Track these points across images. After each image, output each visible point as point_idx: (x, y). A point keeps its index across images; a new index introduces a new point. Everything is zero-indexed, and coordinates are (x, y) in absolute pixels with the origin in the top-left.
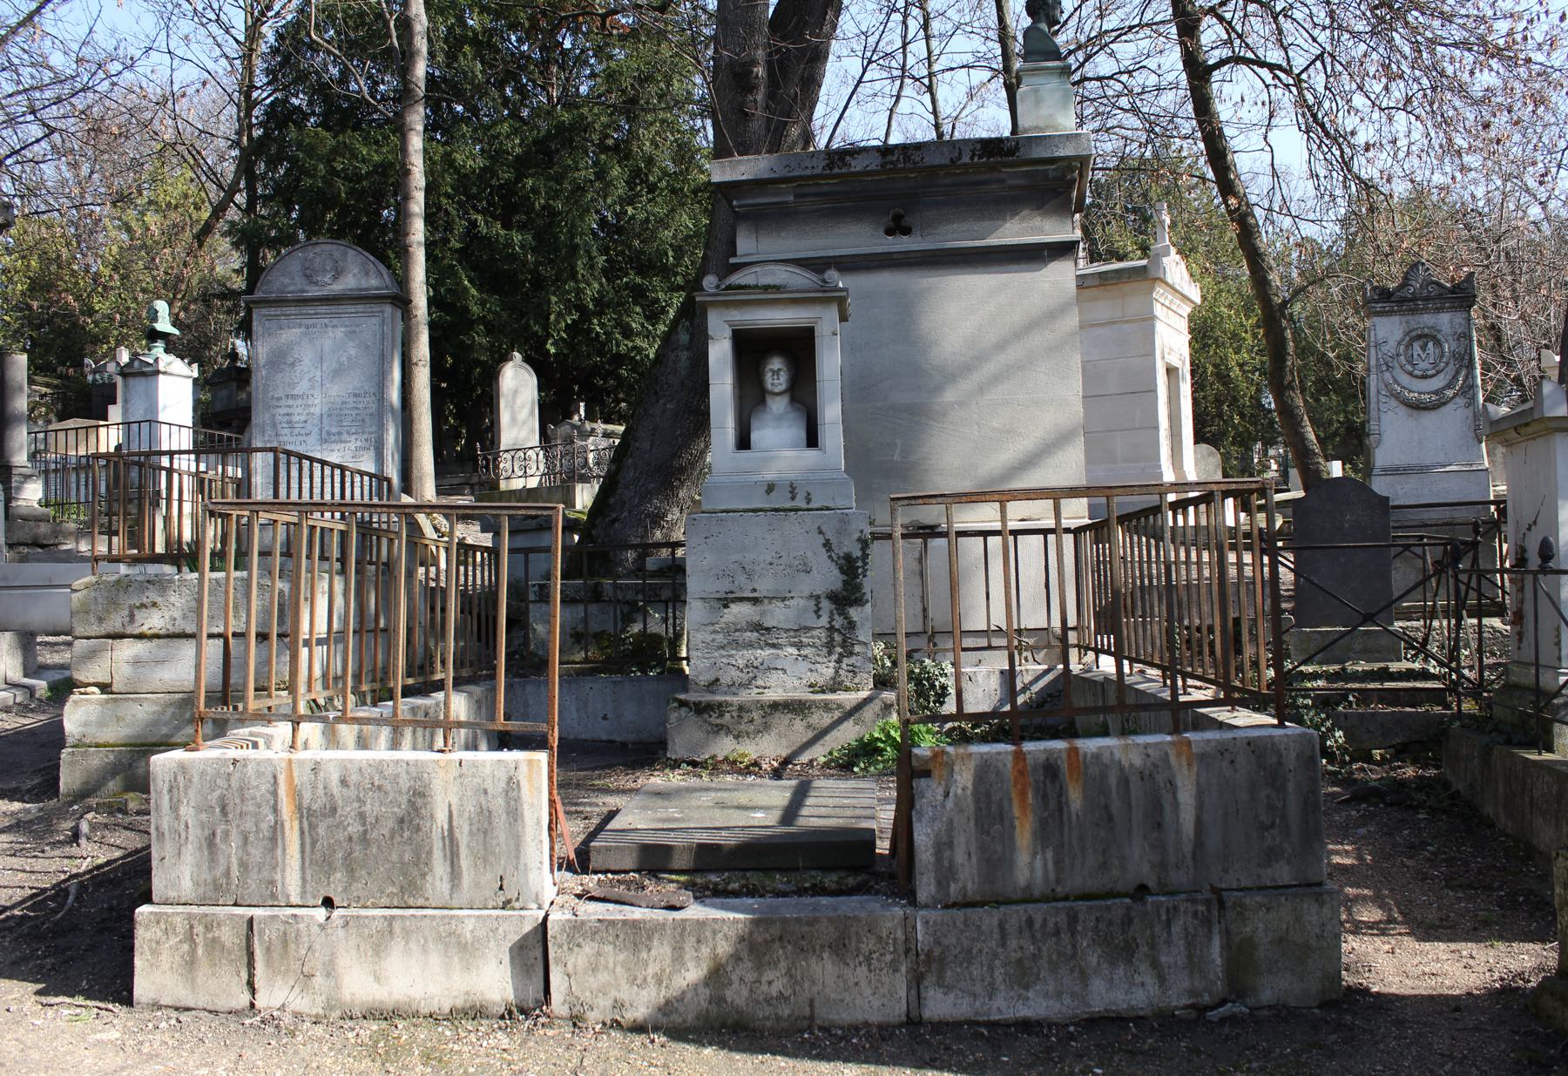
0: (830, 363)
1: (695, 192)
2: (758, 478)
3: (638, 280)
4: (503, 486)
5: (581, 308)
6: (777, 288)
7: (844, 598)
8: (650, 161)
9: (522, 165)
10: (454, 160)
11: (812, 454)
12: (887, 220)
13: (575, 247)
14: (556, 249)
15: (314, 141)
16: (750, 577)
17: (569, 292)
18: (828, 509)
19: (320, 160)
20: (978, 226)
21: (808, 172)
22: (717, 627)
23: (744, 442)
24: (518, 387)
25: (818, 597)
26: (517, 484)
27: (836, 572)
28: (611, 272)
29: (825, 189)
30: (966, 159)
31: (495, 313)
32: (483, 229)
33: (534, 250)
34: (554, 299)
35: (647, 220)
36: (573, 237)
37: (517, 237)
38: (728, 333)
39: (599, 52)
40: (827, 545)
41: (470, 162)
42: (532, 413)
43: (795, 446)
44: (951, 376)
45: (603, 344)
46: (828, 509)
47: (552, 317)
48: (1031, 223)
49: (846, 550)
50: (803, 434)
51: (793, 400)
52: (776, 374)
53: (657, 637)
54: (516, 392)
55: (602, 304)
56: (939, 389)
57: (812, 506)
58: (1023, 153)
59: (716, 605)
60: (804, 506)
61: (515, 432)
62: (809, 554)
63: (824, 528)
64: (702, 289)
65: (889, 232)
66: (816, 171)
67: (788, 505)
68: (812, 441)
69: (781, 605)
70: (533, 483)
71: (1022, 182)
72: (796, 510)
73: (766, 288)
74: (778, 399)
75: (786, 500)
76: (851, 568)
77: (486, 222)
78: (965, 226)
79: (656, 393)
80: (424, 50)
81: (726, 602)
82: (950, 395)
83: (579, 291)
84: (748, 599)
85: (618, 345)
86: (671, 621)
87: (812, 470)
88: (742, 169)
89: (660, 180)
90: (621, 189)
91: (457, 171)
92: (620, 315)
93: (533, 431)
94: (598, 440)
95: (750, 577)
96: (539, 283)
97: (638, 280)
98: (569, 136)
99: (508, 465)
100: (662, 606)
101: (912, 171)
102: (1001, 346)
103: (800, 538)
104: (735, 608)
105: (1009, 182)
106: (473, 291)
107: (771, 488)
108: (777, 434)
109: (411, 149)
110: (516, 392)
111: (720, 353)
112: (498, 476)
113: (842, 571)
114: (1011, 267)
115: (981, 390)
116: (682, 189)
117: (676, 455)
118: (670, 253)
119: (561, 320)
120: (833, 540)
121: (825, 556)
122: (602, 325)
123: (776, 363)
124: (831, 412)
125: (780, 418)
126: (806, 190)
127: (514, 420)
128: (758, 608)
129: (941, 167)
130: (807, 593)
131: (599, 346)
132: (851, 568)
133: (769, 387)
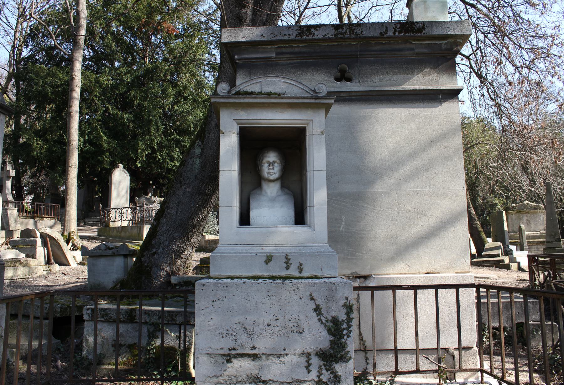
0: (317, 158)
1: (204, 101)
3: (178, 137)
4: (111, 224)
5: (153, 148)
6: (278, 95)
7: (331, 355)
8: (185, 88)
9: (131, 86)
10: (99, 81)
11: (300, 230)
13: (151, 121)
14: (143, 123)
15: (38, 70)
16: (250, 335)
17: (147, 140)
18: (317, 277)
19: (41, 78)
20: (396, 78)
21: (286, 38)
24: (121, 180)
25: (308, 355)
26: (118, 224)
27: (325, 333)
28: (166, 133)
29: (296, 50)
30: (390, 33)
31: (115, 148)
32: (111, 111)
33: (133, 122)
34: (141, 143)
35: (183, 111)
36: (149, 116)
37: (126, 116)
38: (236, 129)
39: (165, 43)
40: (317, 309)
41: (107, 82)
42: (127, 192)
43: (286, 224)
44: (377, 174)
45: (161, 164)
46: (317, 277)
47: (139, 151)
48: (430, 77)
49: (333, 314)
51: (283, 186)
52: (271, 165)
53: (172, 349)
54: (120, 182)
55: (161, 146)
56: (371, 183)
57: (304, 274)
58: (427, 31)
59: (220, 360)
60: (297, 274)
61: (118, 200)
62: (302, 317)
63: (315, 296)
65: (337, 79)
66: (292, 37)
67: (283, 273)
68: (300, 218)
69: (276, 360)
70: (125, 224)
71: (425, 51)
72: (291, 278)
73: (269, 94)
74: (272, 184)
75: (282, 271)
76: (337, 330)
77: (112, 109)
78: (388, 77)
79: (181, 182)
81: (228, 358)
82: (379, 187)
83: (152, 141)
84: (248, 355)
85: (168, 164)
86: (182, 338)
87: (304, 245)
88: (243, 34)
89: (189, 96)
90: (172, 98)
91: (101, 86)
92: (169, 151)
93: (127, 200)
94: (155, 204)
95: (250, 335)
96: (135, 136)
97: (178, 137)
98: (151, 74)
99: (114, 215)
100: (177, 328)
101: (354, 39)
102: (413, 155)
103: (294, 302)
104: (236, 363)
105: (416, 51)
106: (105, 138)
107: (269, 259)
108: (271, 210)
109: (75, 69)
110: (120, 182)
111: (229, 145)
112: (109, 220)
113: (330, 332)
114: (418, 104)
115: (400, 184)
116: (198, 100)
117: (191, 218)
118: (192, 126)
119: (143, 151)
120: (323, 305)
121: (315, 319)
122: (161, 155)
123: (272, 157)
124: (318, 197)
126: (284, 50)
127: (118, 195)
128: (257, 363)
129: (374, 38)
130: (299, 351)
131: (160, 165)
132: (337, 330)
133: (266, 175)
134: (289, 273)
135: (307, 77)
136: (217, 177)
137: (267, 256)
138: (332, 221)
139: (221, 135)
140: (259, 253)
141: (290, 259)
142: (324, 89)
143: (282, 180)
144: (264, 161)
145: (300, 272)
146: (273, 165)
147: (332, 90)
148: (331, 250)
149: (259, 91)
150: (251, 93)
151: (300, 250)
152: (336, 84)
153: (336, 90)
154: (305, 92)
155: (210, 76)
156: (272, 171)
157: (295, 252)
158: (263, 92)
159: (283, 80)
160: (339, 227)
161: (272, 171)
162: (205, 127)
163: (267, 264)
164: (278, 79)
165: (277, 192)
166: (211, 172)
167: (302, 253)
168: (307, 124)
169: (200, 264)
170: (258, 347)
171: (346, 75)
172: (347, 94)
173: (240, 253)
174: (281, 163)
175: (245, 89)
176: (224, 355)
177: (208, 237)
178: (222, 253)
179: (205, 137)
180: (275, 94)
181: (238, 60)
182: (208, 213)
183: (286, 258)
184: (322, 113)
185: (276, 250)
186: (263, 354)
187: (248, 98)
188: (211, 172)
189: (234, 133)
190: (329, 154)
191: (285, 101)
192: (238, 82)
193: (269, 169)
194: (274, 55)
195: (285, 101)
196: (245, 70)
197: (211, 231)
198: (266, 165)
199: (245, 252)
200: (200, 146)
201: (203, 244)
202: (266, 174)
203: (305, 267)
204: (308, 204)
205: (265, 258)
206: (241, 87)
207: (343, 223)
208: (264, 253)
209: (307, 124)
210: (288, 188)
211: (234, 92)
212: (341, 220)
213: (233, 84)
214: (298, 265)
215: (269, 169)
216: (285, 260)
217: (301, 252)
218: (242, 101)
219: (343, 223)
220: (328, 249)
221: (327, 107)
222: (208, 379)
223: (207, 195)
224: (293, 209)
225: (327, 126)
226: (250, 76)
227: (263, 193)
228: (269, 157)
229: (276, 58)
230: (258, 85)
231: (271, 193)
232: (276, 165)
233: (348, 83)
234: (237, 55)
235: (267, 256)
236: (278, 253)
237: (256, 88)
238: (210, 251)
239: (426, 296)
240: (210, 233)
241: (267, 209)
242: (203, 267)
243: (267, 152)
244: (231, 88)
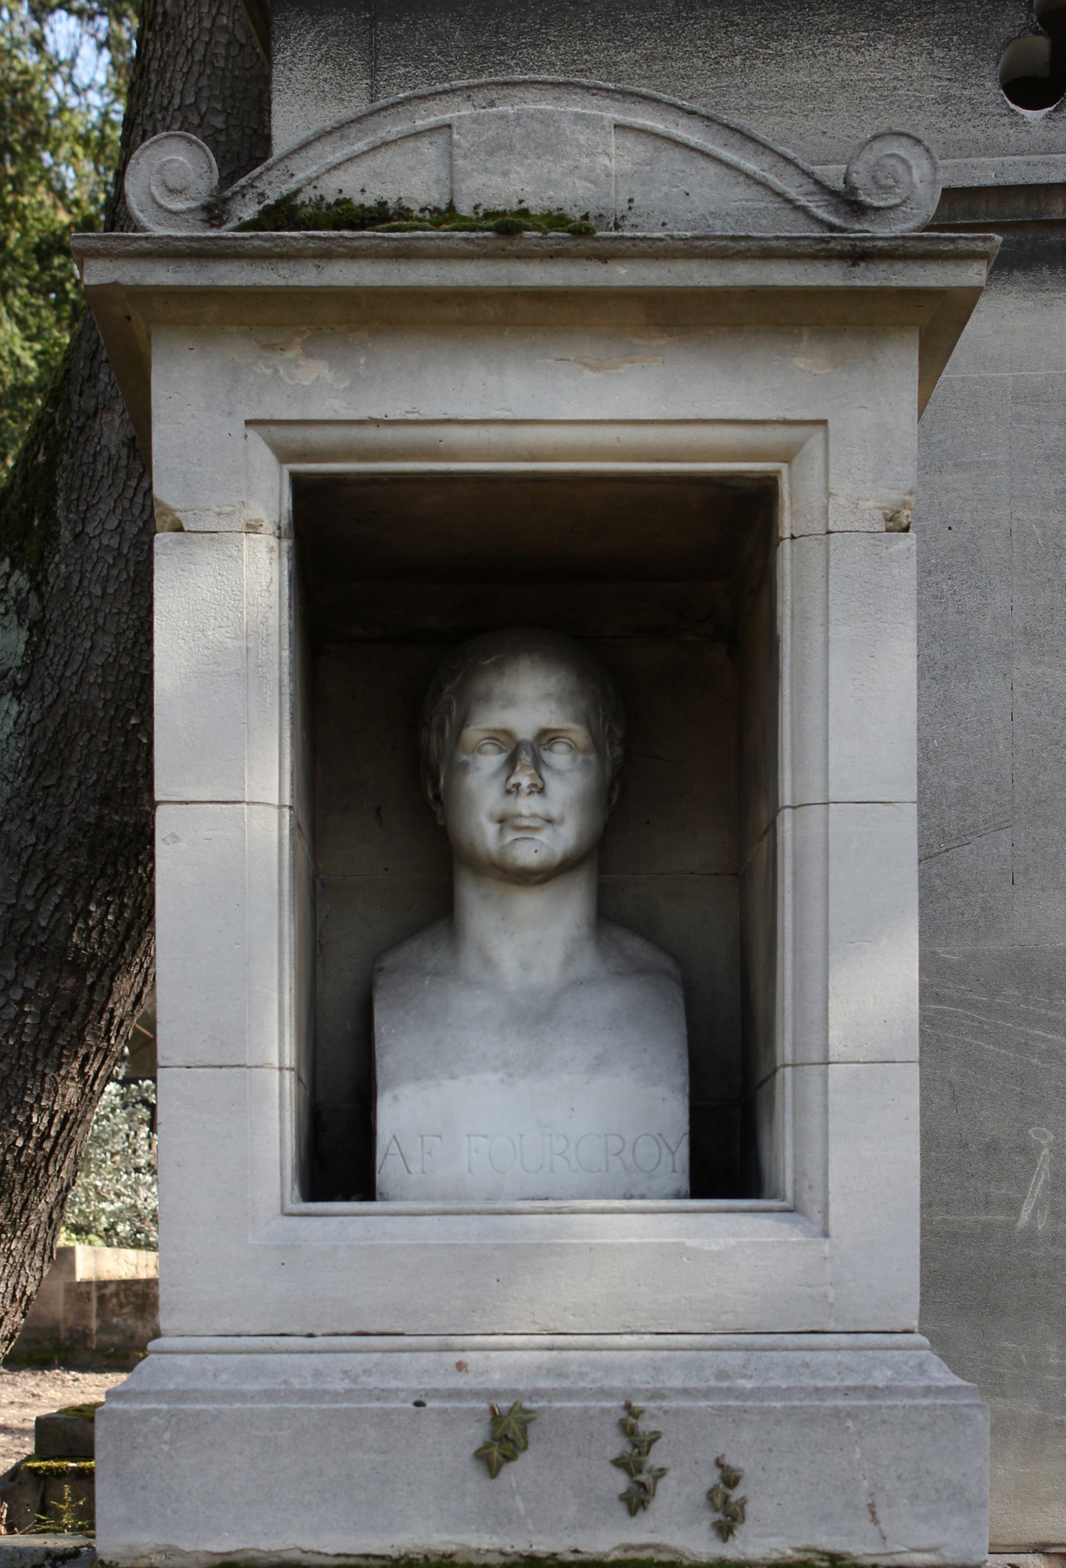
0: (855, 707)
2: (420, 1370)
6: (576, 233)
11: (726, 1231)
23: (338, 1157)
38: (270, 499)
50: (672, 1112)
51: (608, 917)
52: (525, 761)
65: (1026, 90)
68: (728, 1152)
73: (507, 228)
74: (529, 903)
87: (754, 1336)
107: (505, 1438)
108: (525, 1087)
111: (220, 611)
123: (528, 700)
124: (858, 989)
125: (538, 1015)
133: (484, 832)
134: (645, 1538)
135: (801, 76)
136: (141, 841)
137: (496, 1417)
138: (956, 1162)
139: (162, 541)
140: (436, 1393)
141: (655, 1436)
142: (914, 186)
143: (603, 869)
144: (473, 734)
145: (725, 1530)
146: (538, 763)
147: (986, 171)
148: (942, 1375)
149: (437, 198)
150: (379, 216)
151: (722, 1375)
152: (1018, 123)
153: (1012, 178)
154: (773, 204)
155: (88, 50)
156: (527, 805)
157: (686, 1392)
158: (464, 208)
159: (613, 113)
160: (1013, 1207)
161: (527, 805)
162: (52, 463)
163: (493, 1471)
164: (576, 105)
165: (569, 960)
166: (105, 800)
167: (742, 1394)
168: (787, 455)
169: (41, 1453)
173: (305, 1395)
174: (597, 745)
175: (331, 188)
177: (96, 1262)
178: (182, 1395)
179: (50, 536)
180: (556, 220)
182: (89, 1097)
183: (628, 1430)
184: (899, 362)
185: (558, 1372)
187: (354, 255)
188: (105, 800)
189: (252, 528)
190: (939, 671)
191: (622, 275)
192: (290, 120)
193: (512, 791)
195: (622, 275)
196: (331, 21)
197: (117, 1216)
198: (490, 761)
199: (340, 1385)
200: (21, 608)
201: (58, 1308)
202: (491, 830)
203: (757, 1499)
204: (786, 1048)
205: (477, 1434)
206: (304, 169)
207: (1042, 1176)
208: (476, 1394)
209: (787, 455)
210: (646, 928)
211: (249, 211)
212: (1028, 1152)
213: (242, 145)
214: (712, 1478)
215: (512, 791)
216: (618, 1446)
217: (729, 1392)
218: (308, 276)
219: (1042, 1176)
220: (921, 1368)
221: (937, 324)
223: (78, 971)
224: (681, 1079)
225: (933, 459)
226: (373, 72)
227: (471, 964)
228: (510, 702)
230: (429, 150)
231: (526, 966)
232: (559, 758)
235: (496, 1417)
236: (569, 1394)
237: (407, 178)
238: (120, 1356)
240: (109, 1236)
241: (492, 1078)
242: (60, 1475)
243: (499, 667)
244: (227, 180)
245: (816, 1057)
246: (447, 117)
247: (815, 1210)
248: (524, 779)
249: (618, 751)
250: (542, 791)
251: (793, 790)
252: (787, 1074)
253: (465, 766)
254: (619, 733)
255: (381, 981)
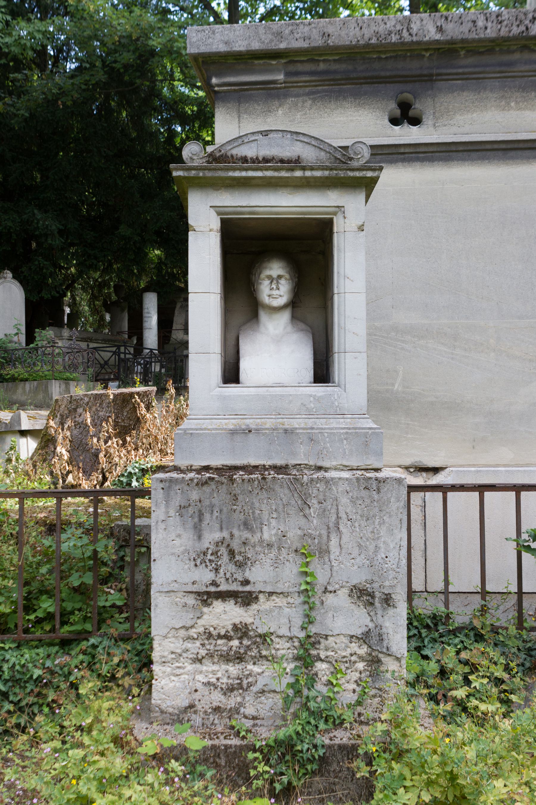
12: (393, 106)
22: (193, 632)
23: (231, 374)
38: (216, 224)
51: (294, 318)
52: (275, 285)
59: (191, 600)
64: (180, 160)
65: (394, 121)
68: (322, 373)
80: (335, 172)
104: (218, 606)
108: (276, 354)
114: (472, 160)
123: (276, 269)
125: (278, 340)
139: (190, 233)
143: (293, 307)
144: (262, 276)
146: (278, 283)
160: (393, 385)
170: (252, 580)
171: (411, 113)
172: (342, 247)
174: (291, 279)
176: (198, 594)
181: (218, 85)
186: (261, 592)
193: (272, 289)
194: (281, 77)
204: (336, 349)
210: (303, 321)
221: (368, 185)
222: (173, 632)
226: (239, 117)
227: (262, 328)
228: (271, 269)
229: (285, 82)
232: (283, 281)
233: (414, 129)
234: (217, 76)
239: (463, 504)
243: (269, 261)
245: (342, 350)
246: (256, 138)
247: (343, 387)
248: (274, 286)
249: (297, 280)
250: (278, 289)
251: (338, 348)
252: (336, 355)
253: (261, 283)
254: (297, 276)
255: (241, 332)
